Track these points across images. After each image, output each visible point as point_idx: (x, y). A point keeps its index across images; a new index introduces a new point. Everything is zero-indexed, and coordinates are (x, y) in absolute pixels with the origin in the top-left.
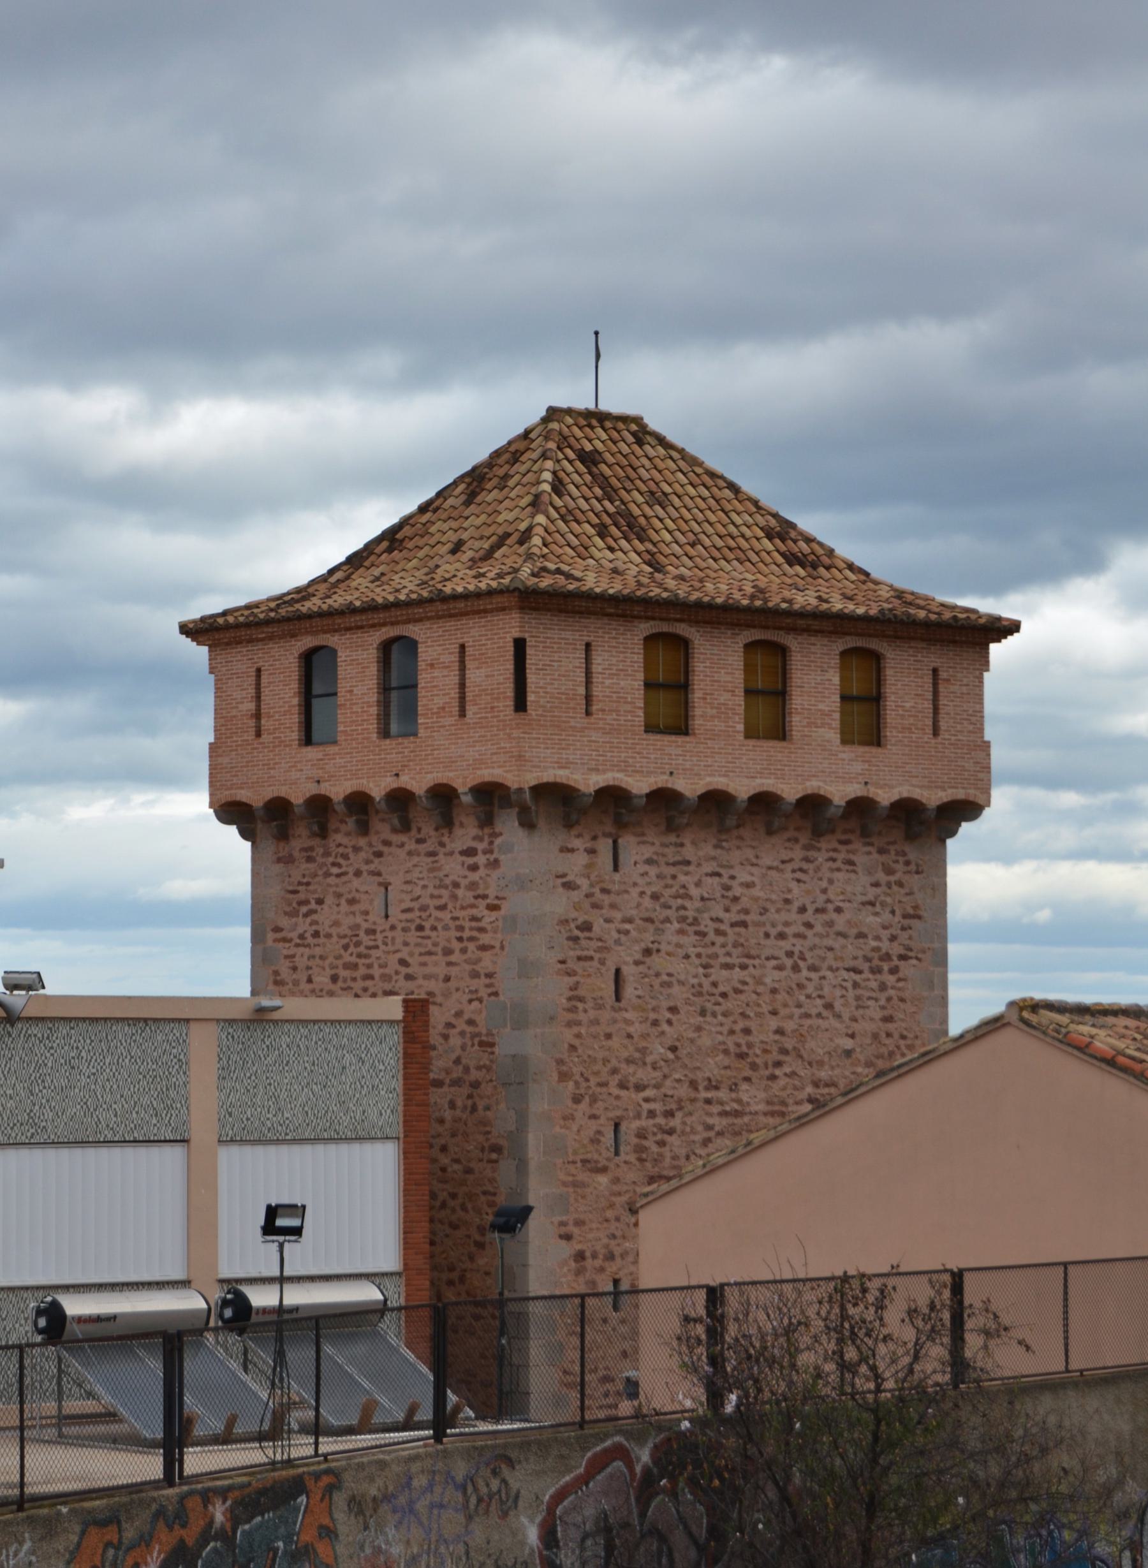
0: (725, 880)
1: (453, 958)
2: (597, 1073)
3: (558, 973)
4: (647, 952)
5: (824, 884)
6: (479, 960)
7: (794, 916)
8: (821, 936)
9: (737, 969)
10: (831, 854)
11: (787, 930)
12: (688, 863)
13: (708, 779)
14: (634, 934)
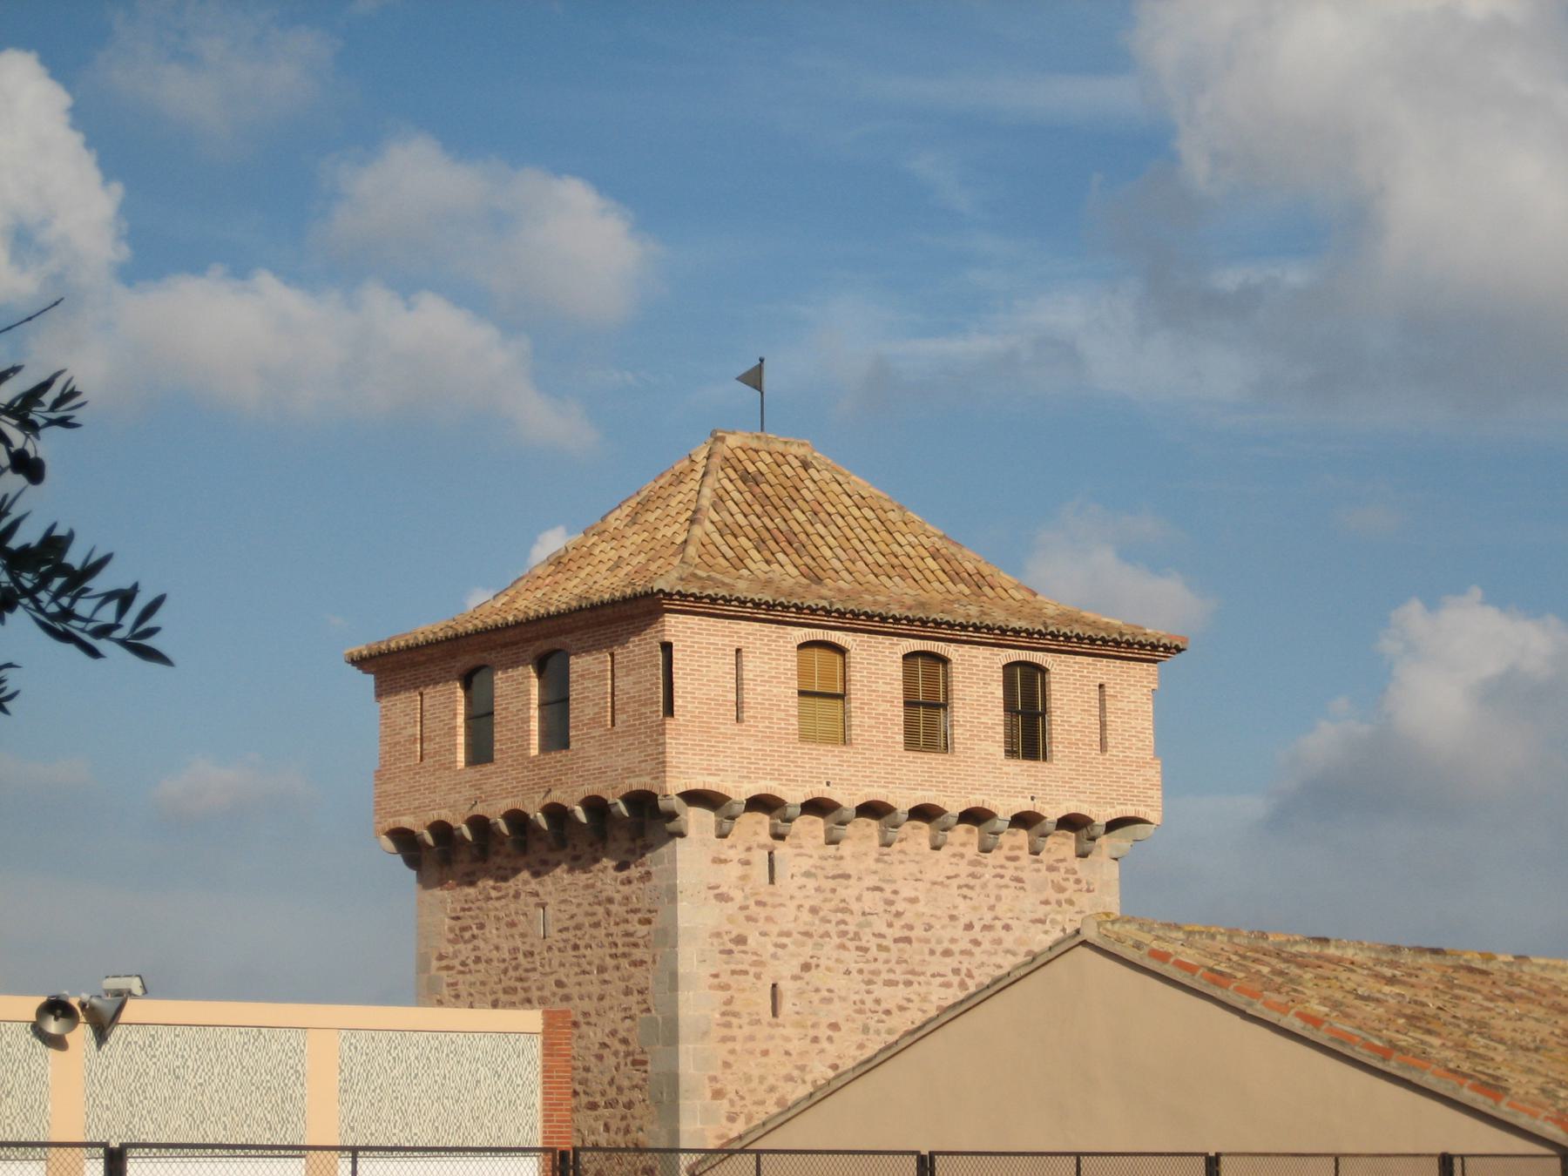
0: (888, 895)
1: (606, 976)
2: (752, 1091)
3: (710, 987)
4: (806, 967)
5: (992, 901)
6: (630, 977)
7: (959, 932)
8: (990, 954)
9: (901, 986)
10: (999, 871)
11: (953, 947)
12: (848, 877)
13: (867, 790)
14: (791, 948)
